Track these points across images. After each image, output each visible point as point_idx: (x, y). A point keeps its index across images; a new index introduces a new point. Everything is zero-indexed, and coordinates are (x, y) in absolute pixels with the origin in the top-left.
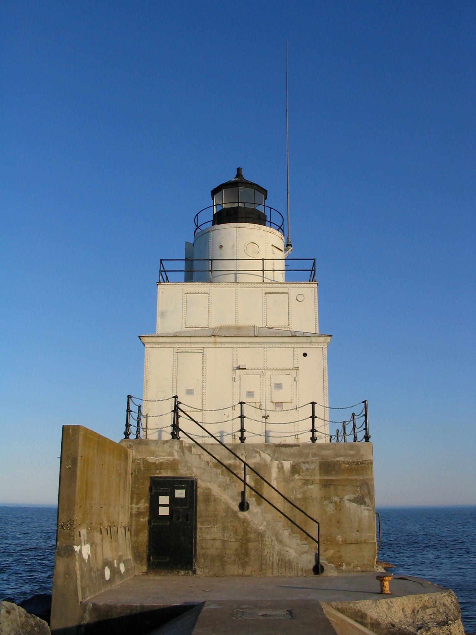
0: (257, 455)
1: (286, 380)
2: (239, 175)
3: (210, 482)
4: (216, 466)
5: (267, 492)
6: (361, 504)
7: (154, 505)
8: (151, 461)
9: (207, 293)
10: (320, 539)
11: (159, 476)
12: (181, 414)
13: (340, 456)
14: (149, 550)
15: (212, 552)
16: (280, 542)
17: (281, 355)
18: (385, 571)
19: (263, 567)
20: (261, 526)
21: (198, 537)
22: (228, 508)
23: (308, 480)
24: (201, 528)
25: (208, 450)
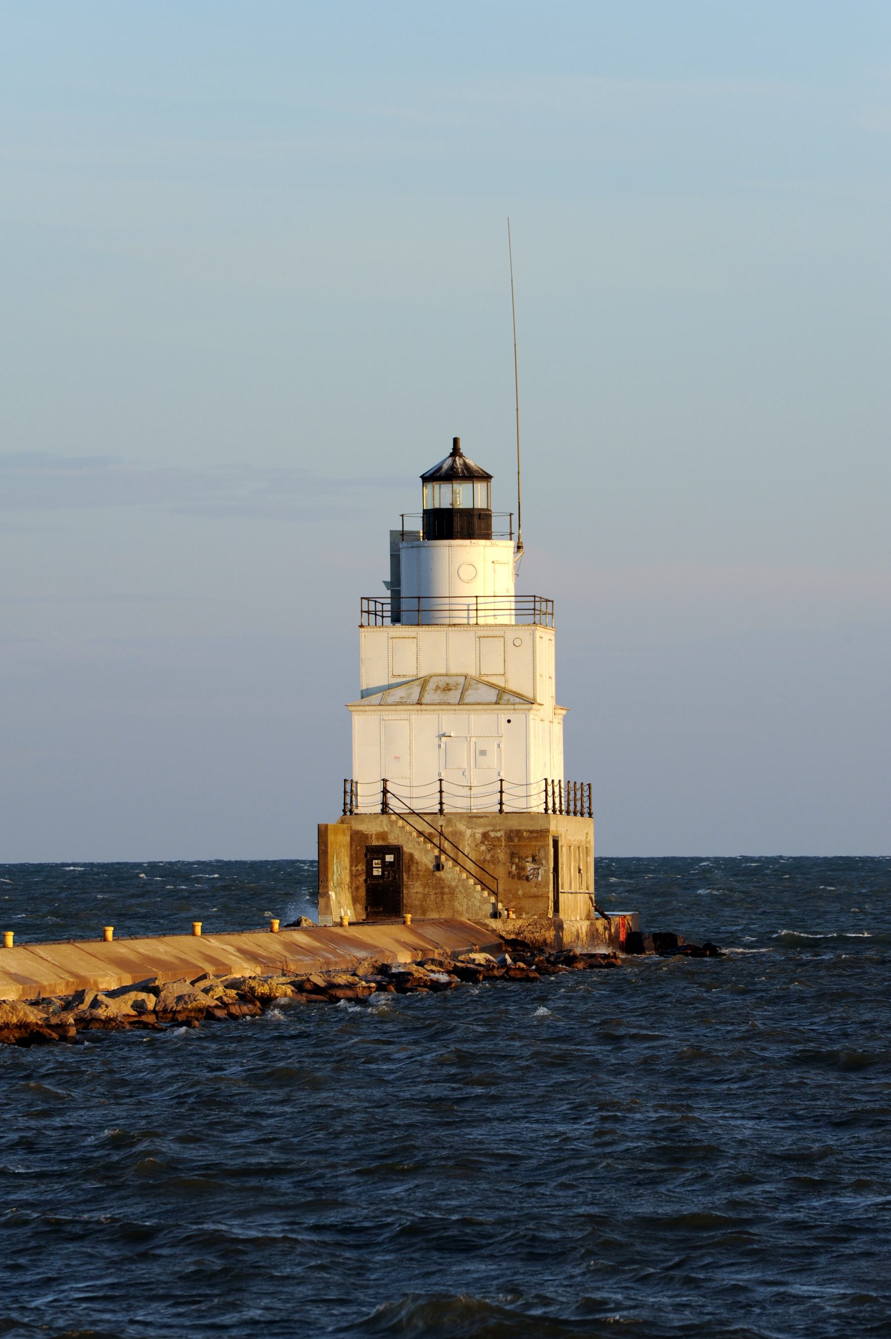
2: (456, 452)
7: (370, 868)
18: (133, 1013)
22: (427, 869)
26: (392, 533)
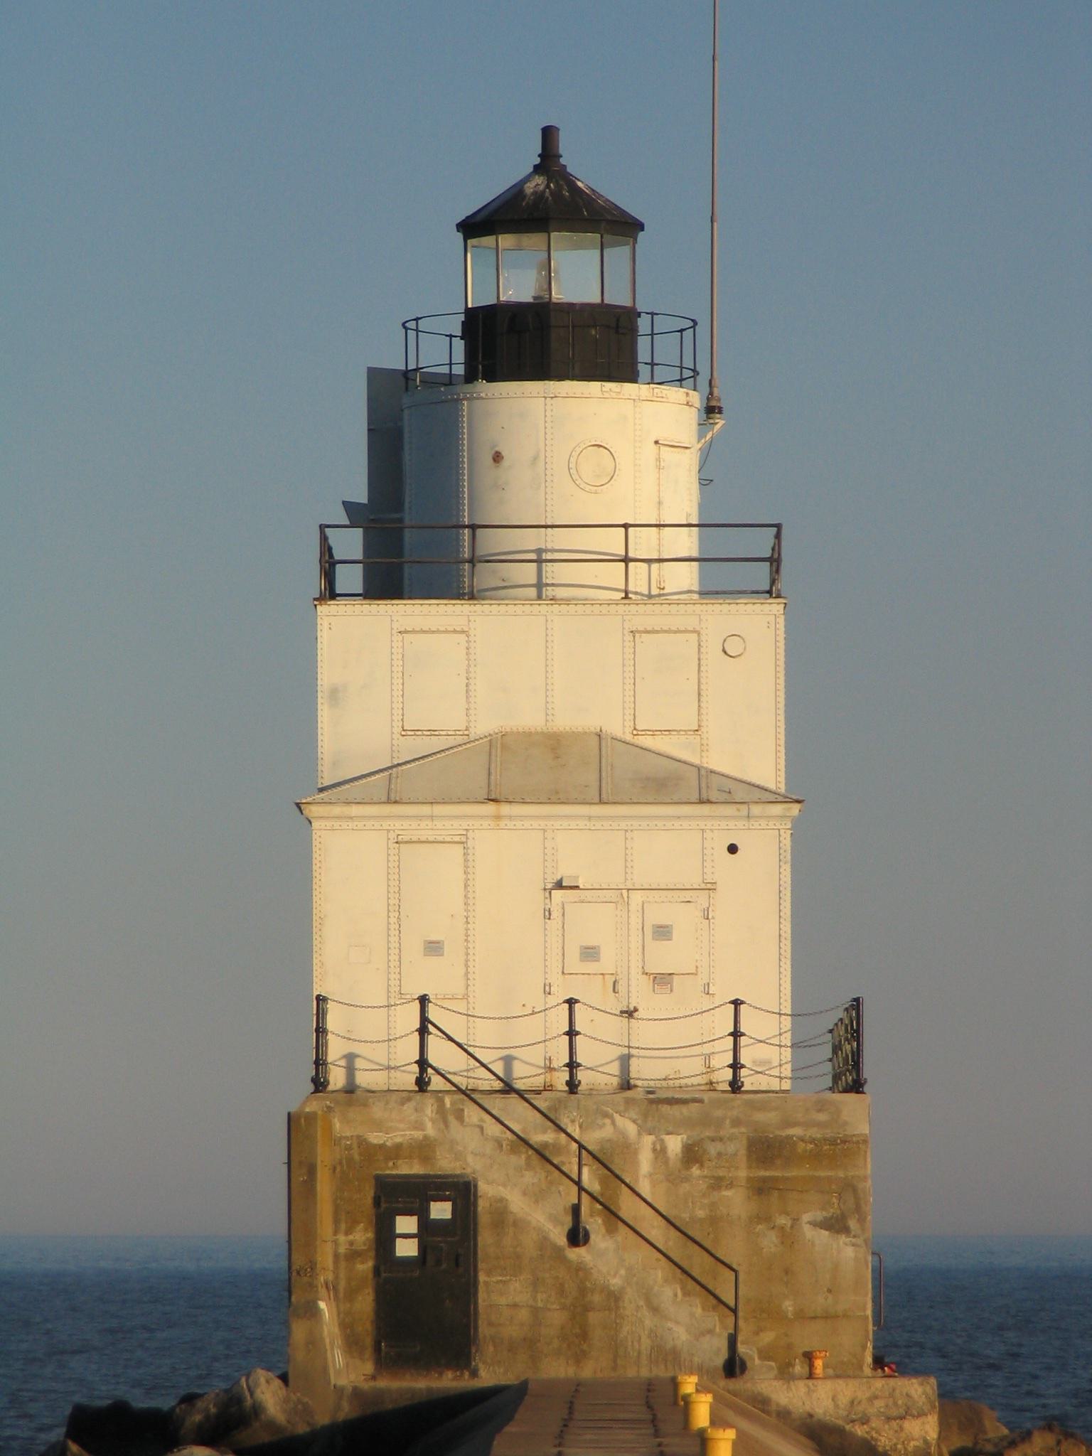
0: (607, 1121)
1: (682, 917)
2: (548, 161)
3: (504, 1185)
4: (513, 1150)
5: (628, 1206)
6: (838, 1232)
7: (385, 1237)
8: (375, 1142)
9: (463, 632)
10: (740, 1307)
11: (394, 1172)
12: (431, 1028)
13: (795, 1124)
14: (378, 1328)
15: (512, 1331)
16: (655, 1310)
17: (667, 845)
19: (619, 1362)
20: (615, 1276)
21: (480, 1301)
22: (544, 1242)
23: (720, 1179)
24: (486, 1283)
25: (494, 1112)
26: (376, 376)
